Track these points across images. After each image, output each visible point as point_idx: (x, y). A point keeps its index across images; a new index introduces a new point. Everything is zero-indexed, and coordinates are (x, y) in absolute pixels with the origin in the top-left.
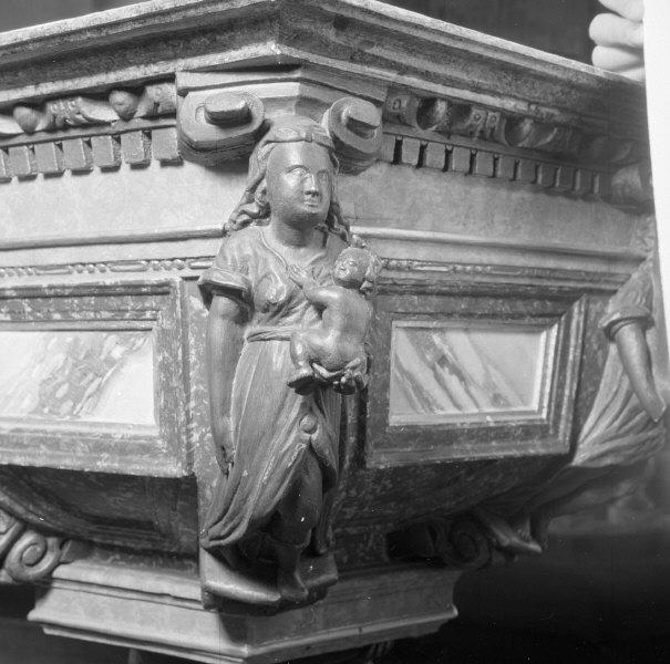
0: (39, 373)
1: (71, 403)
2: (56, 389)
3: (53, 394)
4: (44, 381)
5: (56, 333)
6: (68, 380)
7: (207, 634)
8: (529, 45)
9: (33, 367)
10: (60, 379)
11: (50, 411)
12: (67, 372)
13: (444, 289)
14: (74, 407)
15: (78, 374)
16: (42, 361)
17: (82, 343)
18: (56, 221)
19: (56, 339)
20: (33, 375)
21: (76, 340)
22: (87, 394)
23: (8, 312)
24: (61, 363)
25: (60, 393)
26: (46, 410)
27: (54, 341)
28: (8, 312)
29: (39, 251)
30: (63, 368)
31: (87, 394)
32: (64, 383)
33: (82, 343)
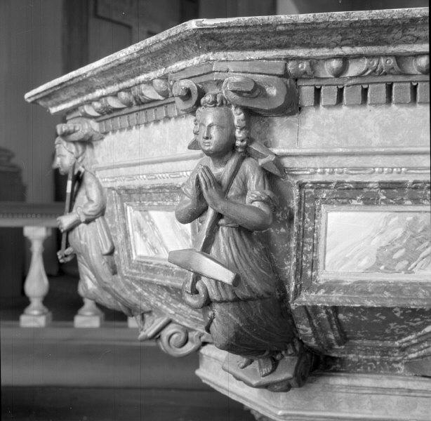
0: (377, 242)
1: (407, 263)
2: (393, 253)
3: (390, 256)
4: (382, 247)
5: (397, 213)
6: (406, 246)
7: (75, 235)
8: (100, 59)
9: (373, 238)
10: (398, 245)
11: (385, 268)
12: (405, 241)
13: (349, 151)
14: (409, 265)
15: (415, 242)
16: (382, 233)
17: (420, 221)
18: (422, 136)
19: (396, 218)
20: (372, 244)
21: (415, 219)
22: (421, 256)
23: (362, 199)
24: (400, 235)
25: (396, 256)
26: (382, 268)
27: (394, 220)
28: (362, 199)
29: (415, 157)
30: (401, 238)
31: (421, 256)
32: (401, 248)
33: (420, 221)
